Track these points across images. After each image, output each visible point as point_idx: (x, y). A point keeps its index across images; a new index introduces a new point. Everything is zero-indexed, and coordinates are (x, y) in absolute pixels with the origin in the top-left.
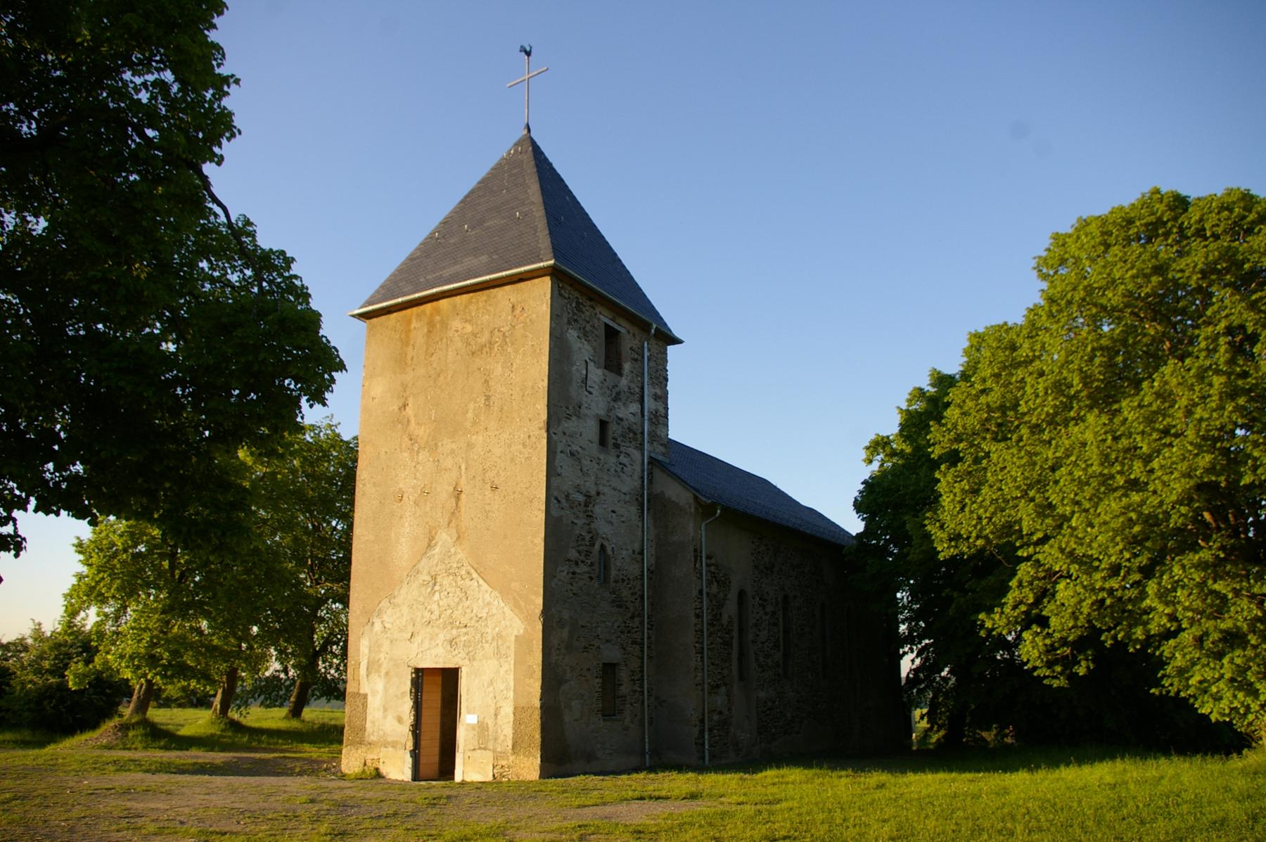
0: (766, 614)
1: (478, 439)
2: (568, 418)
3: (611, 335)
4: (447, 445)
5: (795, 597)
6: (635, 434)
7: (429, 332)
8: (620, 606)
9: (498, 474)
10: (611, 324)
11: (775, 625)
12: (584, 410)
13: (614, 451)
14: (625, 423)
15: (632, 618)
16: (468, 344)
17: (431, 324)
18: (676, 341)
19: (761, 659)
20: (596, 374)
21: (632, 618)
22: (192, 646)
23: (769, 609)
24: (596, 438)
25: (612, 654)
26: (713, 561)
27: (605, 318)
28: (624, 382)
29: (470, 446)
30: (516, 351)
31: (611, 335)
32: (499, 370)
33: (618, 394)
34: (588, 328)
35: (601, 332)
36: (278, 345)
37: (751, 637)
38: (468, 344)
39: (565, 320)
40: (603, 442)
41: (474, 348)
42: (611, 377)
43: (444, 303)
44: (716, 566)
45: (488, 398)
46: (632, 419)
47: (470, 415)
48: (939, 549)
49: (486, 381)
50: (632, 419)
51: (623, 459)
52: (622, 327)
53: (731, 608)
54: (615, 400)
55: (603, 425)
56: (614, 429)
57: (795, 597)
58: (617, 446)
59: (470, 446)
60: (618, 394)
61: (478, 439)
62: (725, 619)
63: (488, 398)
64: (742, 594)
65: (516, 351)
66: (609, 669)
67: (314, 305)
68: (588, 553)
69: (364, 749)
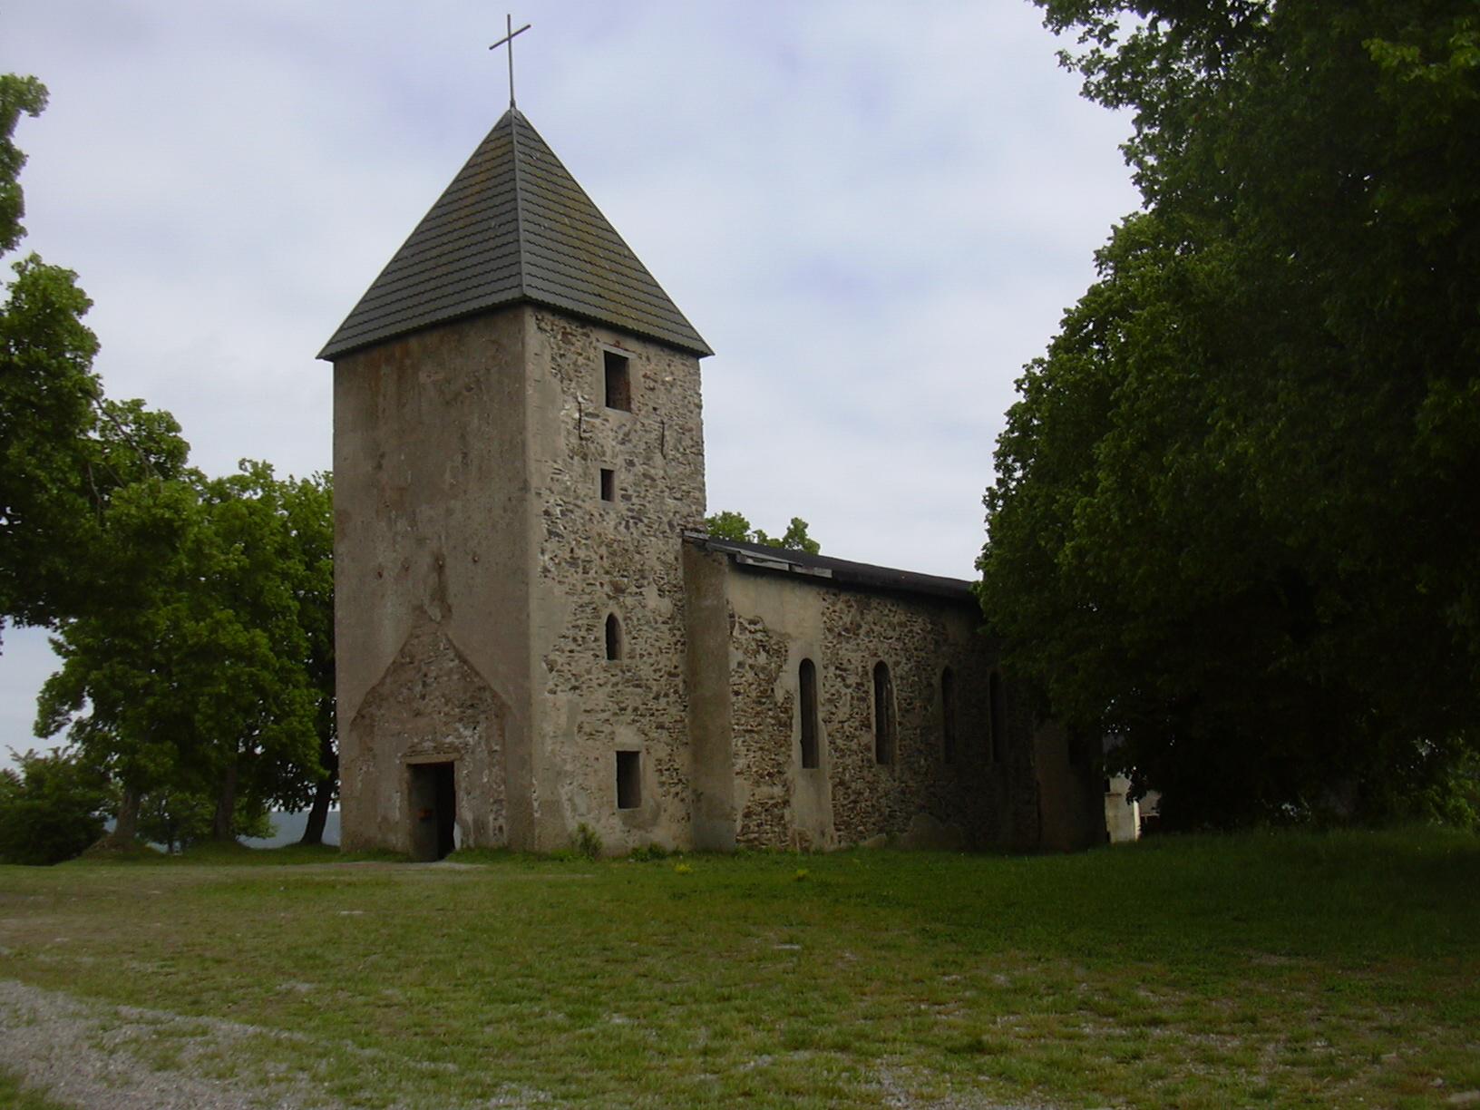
0: (848, 687)
3: (615, 366)
5: (897, 664)
6: (653, 480)
8: (638, 686)
9: (682, 1071)
10: (614, 350)
11: (863, 700)
15: (656, 698)
18: (706, 352)
19: (840, 742)
21: (656, 698)
22: (32, 405)
23: (852, 680)
25: (628, 738)
26: (759, 627)
29: (450, 512)
31: (615, 366)
34: (581, 360)
37: (820, 716)
43: (414, 343)
44: (764, 631)
45: (465, 455)
49: (463, 436)
52: (632, 351)
53: (790, 680)
56: (621, 479)
57: (897, 664)
58: (627, 498)
59: (450, 512)
62: (780, 696)
63: (465, 455)
64: (806, 667)
66: (627, 762)
67: (184, 435)
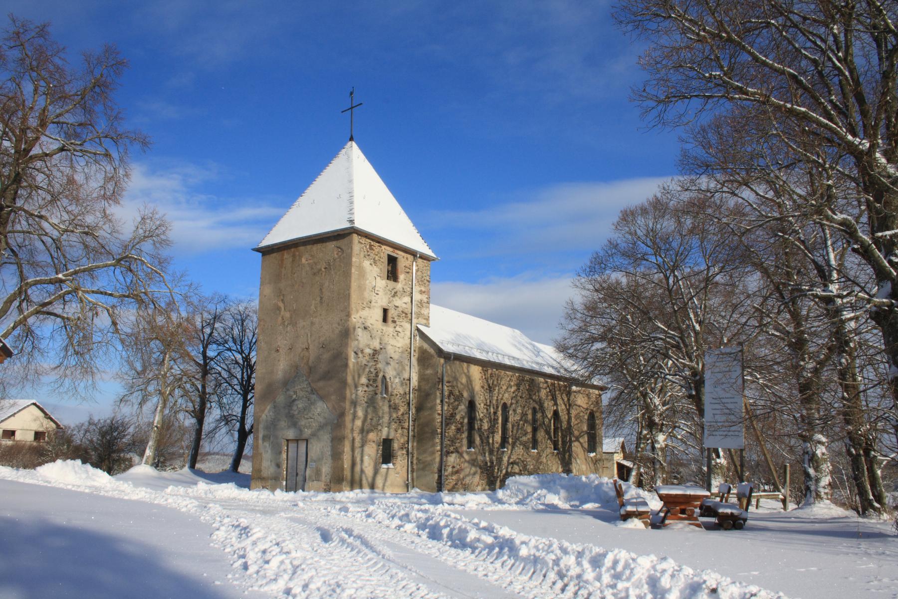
1: (316, 320)
2: (363, 308)
3: (392, 260)
4: (301, 323)
7: (293, 261)
12: (373, 304)
13: (393, 325)
14: (400, 309)
16: (312, 268)
17: (294, 256)
20: (382, 283)
24: (381, 318)
27: (389, 250)
28: (399, 286)
29: (312, 323)
30: (336, 273)
31: (392, 260)
32: (327, 284)
33: (396, 293)
34: (377, 258)
35: (385, 260)
36: (239, 431)
38: (312, 268)
39: (362, 256)
40: (385, 320)
41: (315, 271)
42: (391, 284)
45: (321, 298)
46: (404, 306)
47: (313, 307)
48: (787, 348)
50: (404, 306)
51: (398, 329)
54: (394, 296)
55: (385, 311)
56: (392, 313)
58: (394, 322)
59: (312, 323)
60: (396, 293)
61: (316, 320)
65: (336, 273)
68: (375, 381)
69: (365, 405)
